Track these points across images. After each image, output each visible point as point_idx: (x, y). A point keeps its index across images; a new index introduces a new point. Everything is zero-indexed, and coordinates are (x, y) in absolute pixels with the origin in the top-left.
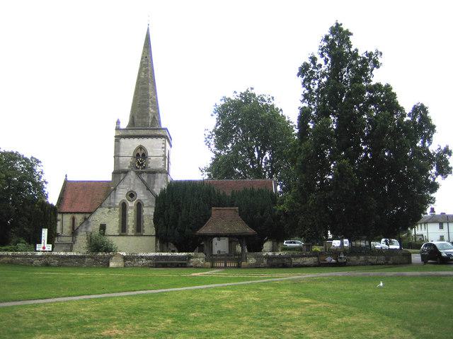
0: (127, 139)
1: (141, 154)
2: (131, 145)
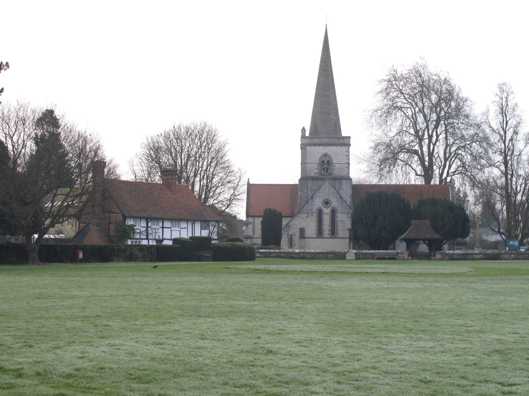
0: (313, 147)
1: (326, 161)
2: (317, 152)
